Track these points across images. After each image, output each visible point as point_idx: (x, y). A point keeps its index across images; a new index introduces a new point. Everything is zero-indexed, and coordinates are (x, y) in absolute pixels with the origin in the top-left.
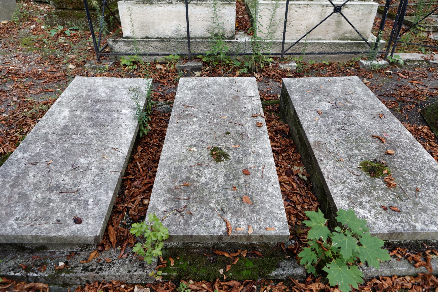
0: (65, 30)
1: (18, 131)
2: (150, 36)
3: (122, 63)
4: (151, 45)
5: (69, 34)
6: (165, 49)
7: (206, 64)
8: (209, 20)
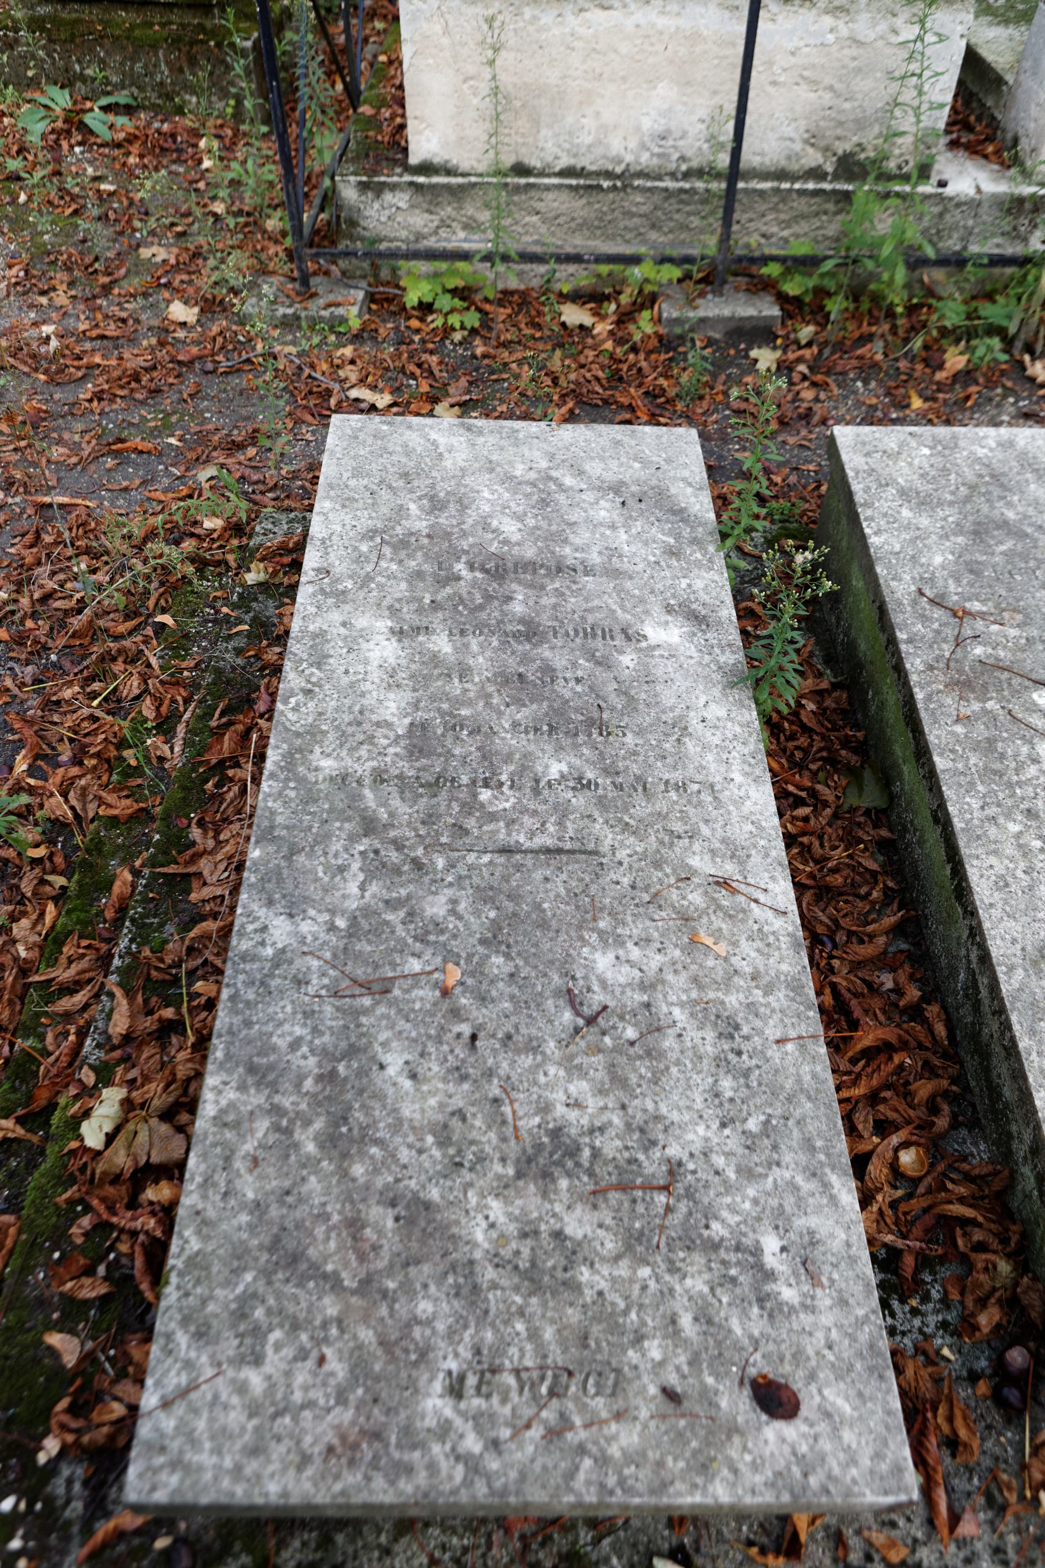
0: (85, 111)
1: (94, 695)
2: (535, 163)
3: (412, 298)
4: (539, 206)
5: (106, 135)
6: (598, 226)
7: (793, 308)
8: (828, 80)
